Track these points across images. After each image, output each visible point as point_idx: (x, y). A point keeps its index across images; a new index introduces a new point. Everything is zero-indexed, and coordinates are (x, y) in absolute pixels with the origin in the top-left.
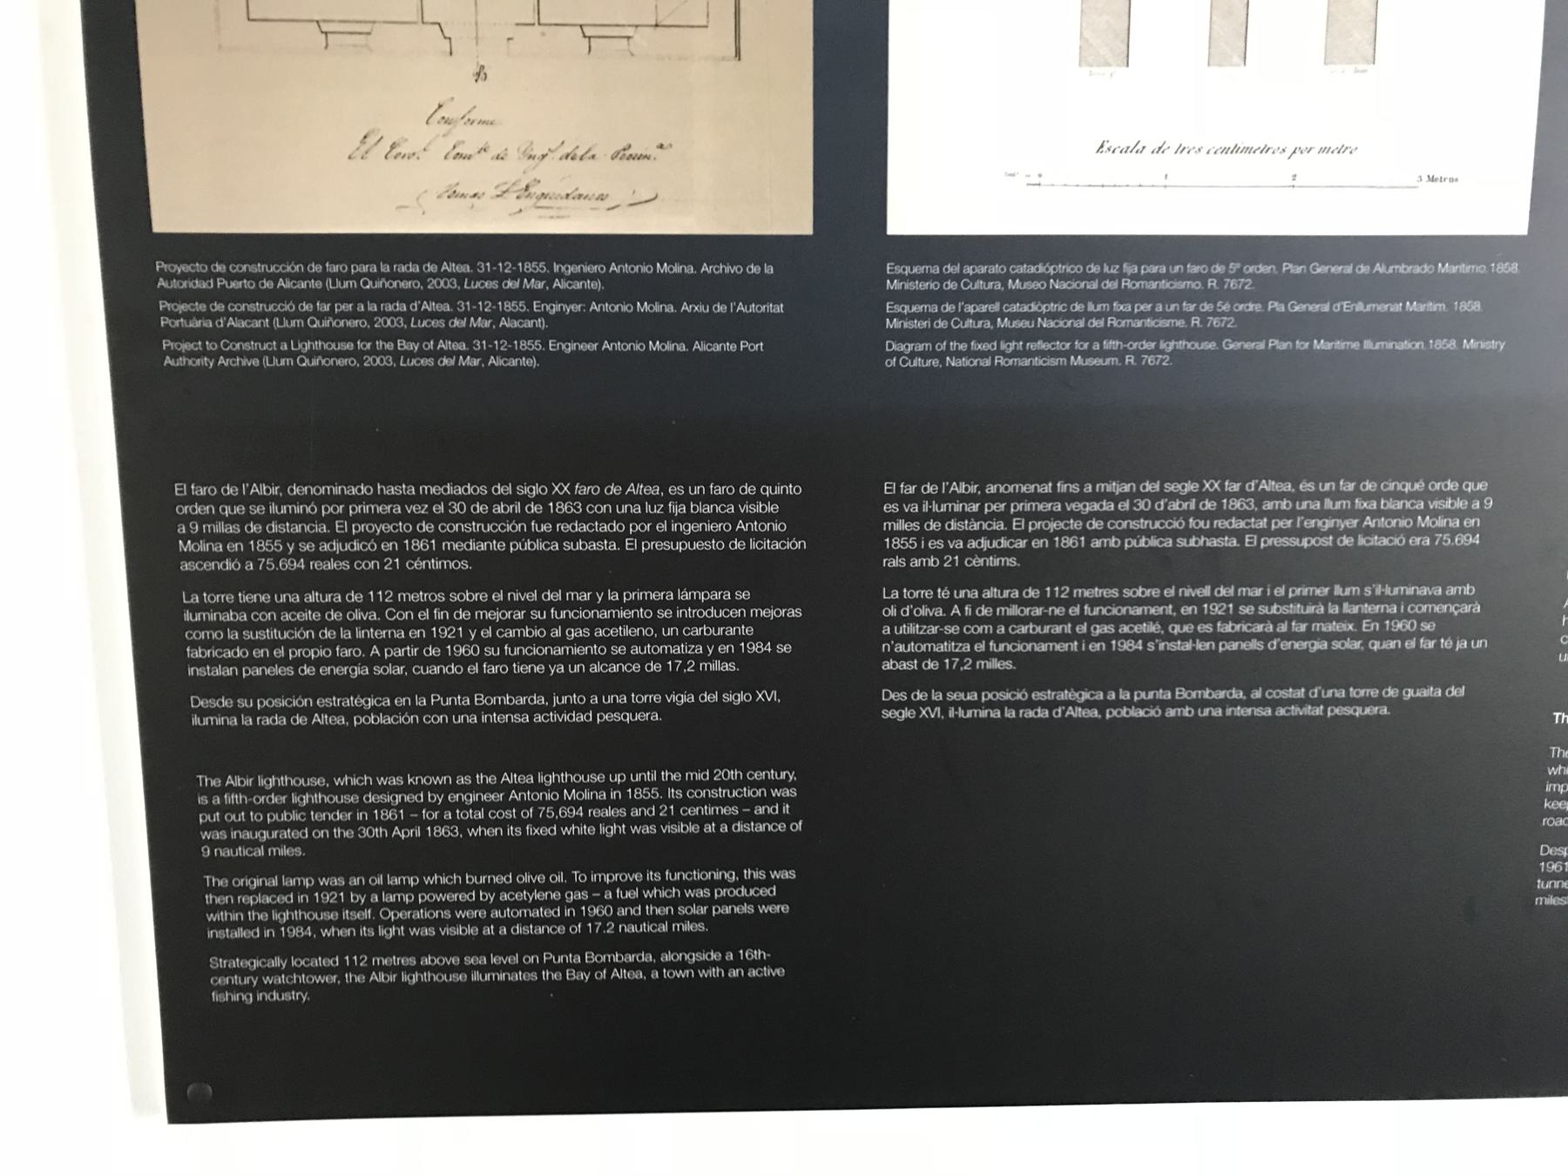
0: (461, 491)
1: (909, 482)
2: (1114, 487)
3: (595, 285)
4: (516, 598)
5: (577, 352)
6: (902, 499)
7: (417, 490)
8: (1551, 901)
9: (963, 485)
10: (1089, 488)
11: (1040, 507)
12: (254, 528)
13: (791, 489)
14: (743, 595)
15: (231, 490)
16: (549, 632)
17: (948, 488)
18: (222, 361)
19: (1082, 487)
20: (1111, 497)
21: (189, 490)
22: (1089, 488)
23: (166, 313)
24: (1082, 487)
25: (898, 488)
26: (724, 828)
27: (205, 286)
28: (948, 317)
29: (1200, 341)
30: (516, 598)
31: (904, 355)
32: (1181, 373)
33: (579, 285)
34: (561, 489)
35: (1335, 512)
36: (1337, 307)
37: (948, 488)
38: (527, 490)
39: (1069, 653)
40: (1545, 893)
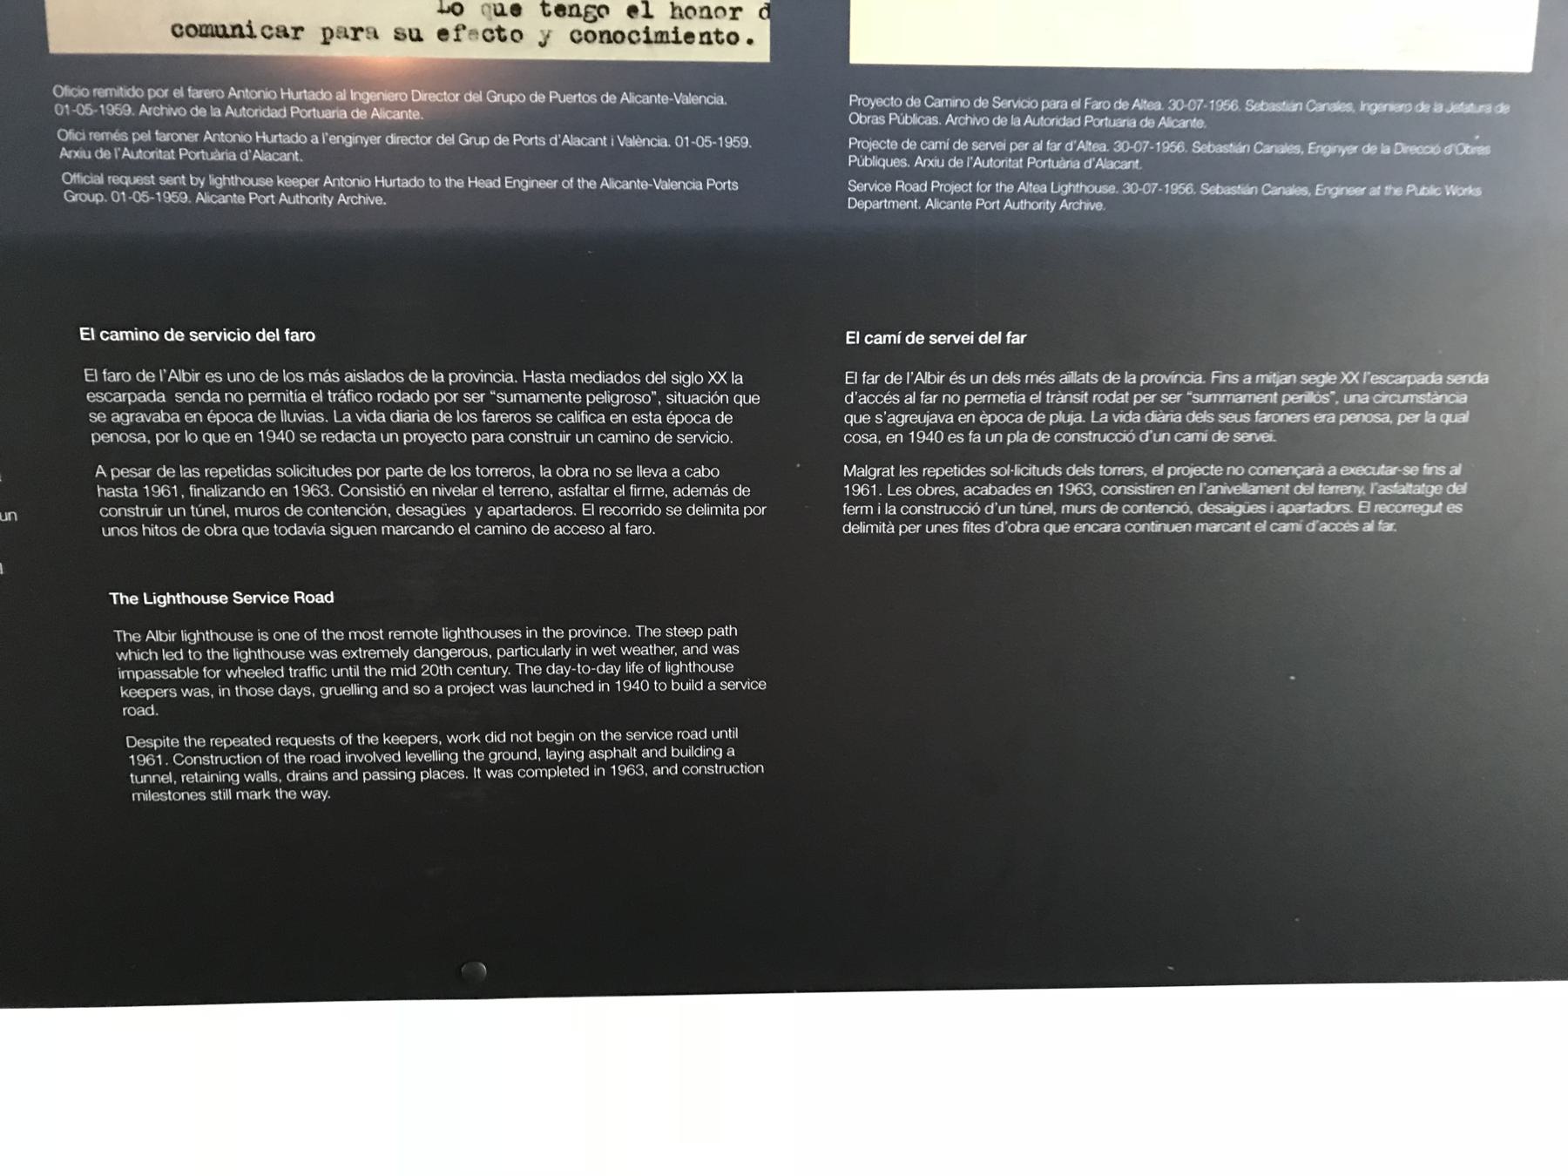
0: (613, 379)
1: (871, 372)
2: (1273, 378)
3: (1198, 123)
4: (441, 493)
5: (534, 190)
6: (864, 389)
7: (567, 378)
8: (149, 796)
9: (928, 375)
10: (1248, 380)
11: (1257, 399)
12: (1037, 418)
13: (1482, 379)
14: (743, 491)
15: (146, 377)
16: (607, 529)
17: (912, 378)
18: (342, 199)
19: (1241, 378)
20: (1267, 389)
21: (101, 376)
22: (1248, 380)
23: (855, 150)
24: (1241, 378)
25: (860, 378)
26: (712, 686)
27: (1072, 123)
28: (961, 155)
29: (1098, 184)
30: (441, 493)
31: (862, 200)
32: (1163, 234)
33: (1184, 124)
34: (717, 377)
35: (1140, 400)
36: (1448, 150)
37: (912, 378)
38: (682, 378)
39: (1242, 533)
40: (142, 788)
